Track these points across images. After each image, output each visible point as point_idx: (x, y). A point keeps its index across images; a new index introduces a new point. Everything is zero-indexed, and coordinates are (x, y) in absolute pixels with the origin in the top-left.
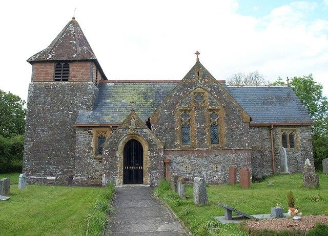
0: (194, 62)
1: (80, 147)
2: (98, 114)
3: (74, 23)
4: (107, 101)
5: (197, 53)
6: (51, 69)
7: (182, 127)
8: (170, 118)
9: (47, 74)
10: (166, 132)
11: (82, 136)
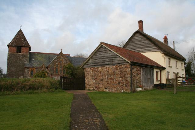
0: (61, 51)
1: (26, 73)
2: (31, 64)
3: (20, 32)
4: (114, 115)
5: (61, 49)
6: (15, 49)
7: (56, 69)
8: (53, 67)
9: (14, 50)
10: (52, 70)
11: (26, 70)
